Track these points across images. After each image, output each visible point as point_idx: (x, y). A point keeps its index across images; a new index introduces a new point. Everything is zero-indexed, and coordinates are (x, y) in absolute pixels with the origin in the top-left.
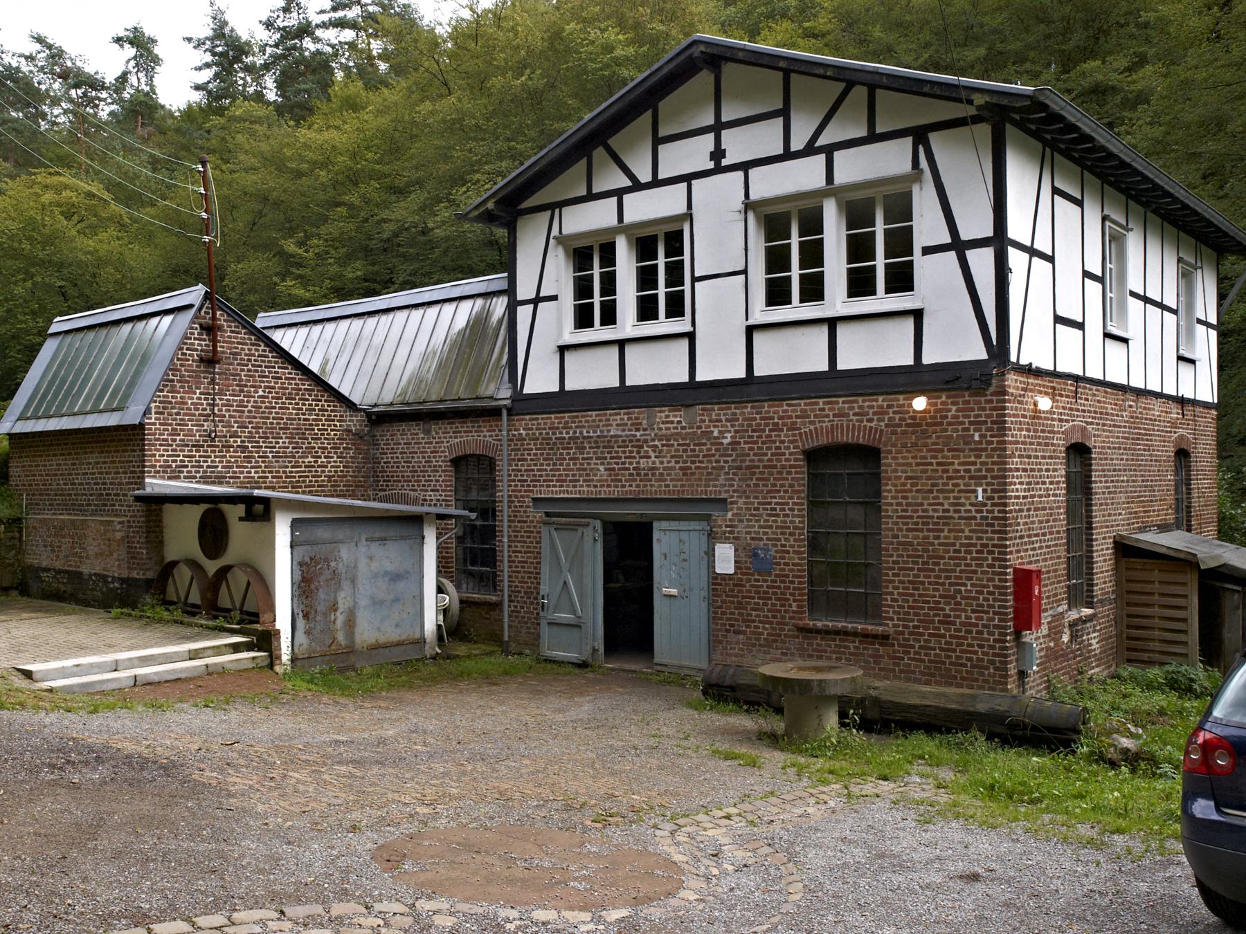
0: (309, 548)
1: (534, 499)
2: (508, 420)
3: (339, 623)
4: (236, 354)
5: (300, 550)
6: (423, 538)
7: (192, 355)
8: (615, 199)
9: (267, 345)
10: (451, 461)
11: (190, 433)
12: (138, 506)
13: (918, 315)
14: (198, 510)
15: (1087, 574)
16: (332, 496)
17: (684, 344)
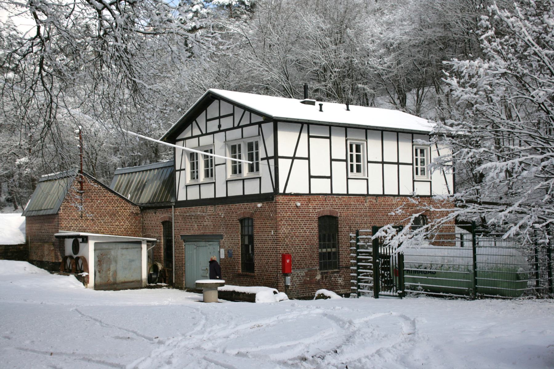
0: (100, 251)
1: (181, 236)
2: (174, 209)
3: (111, 275)
4: (90, 189)
5: (97, 251)
6: (141, 248)
8: (197, 138)
9: (101, 186)
10: (162, 223)
11: (74, 216)
12: (57, 239)
14: (71, 240)
15: (329, 258)
16: (126, 235)
17: (213, 185)
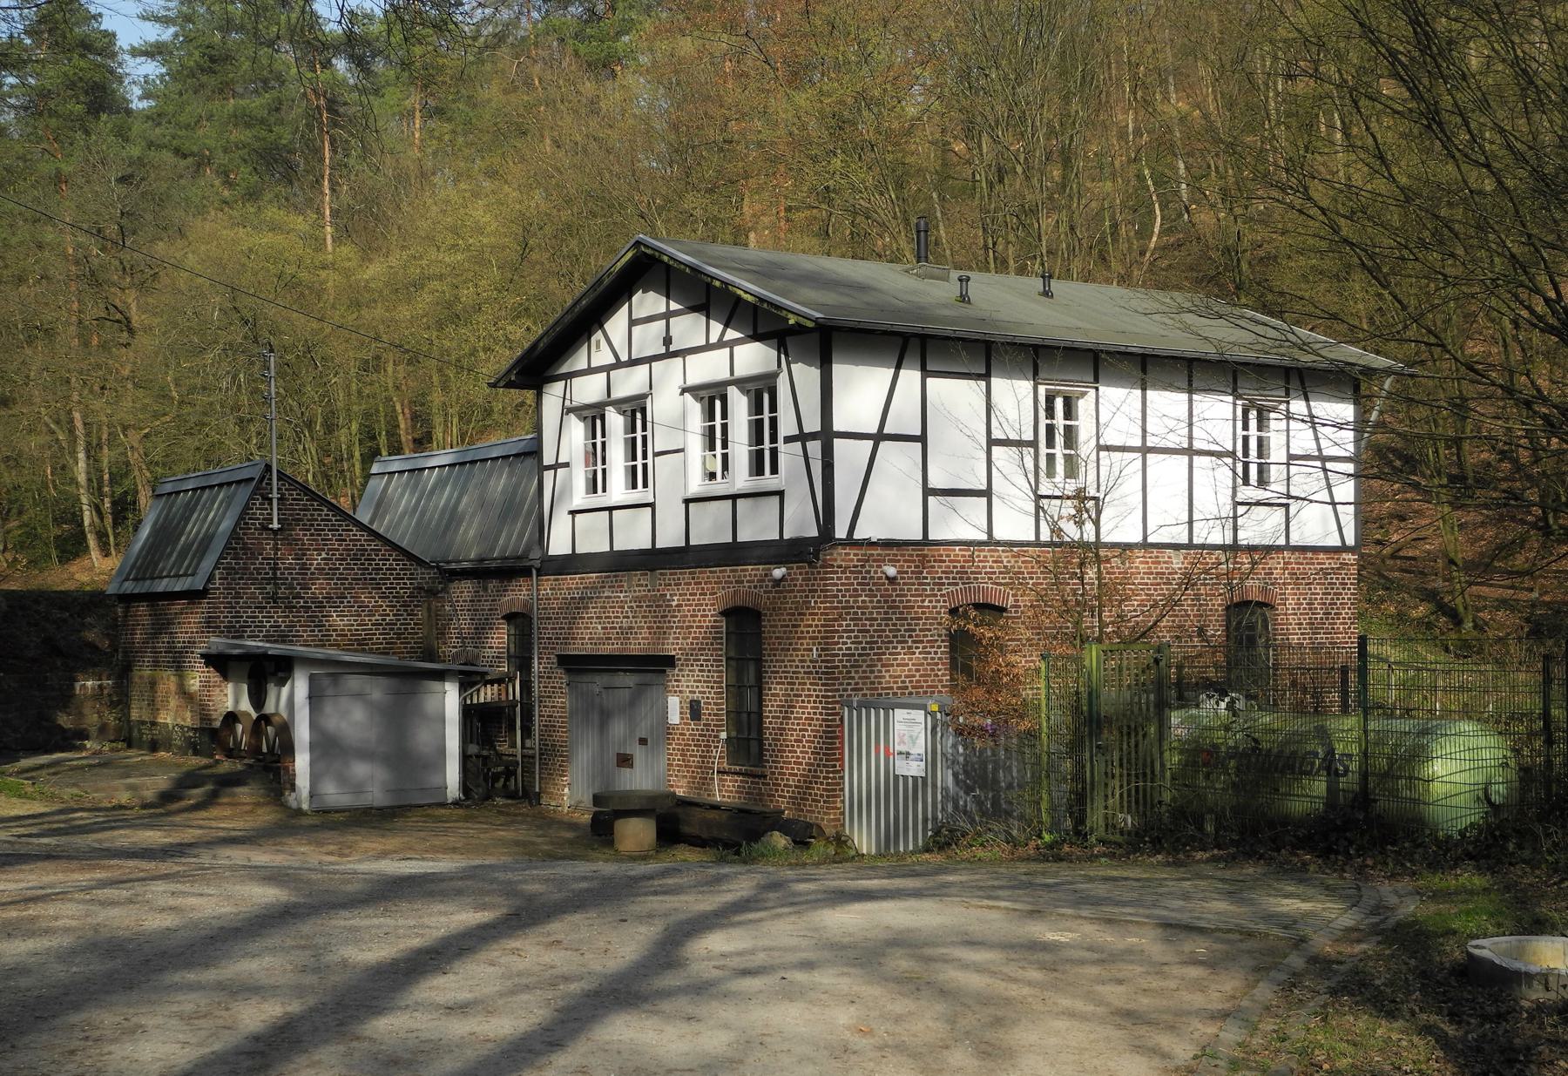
7: (254, 524)
9: (329, 510)
11: (253, 595)
13: (781, 494)
